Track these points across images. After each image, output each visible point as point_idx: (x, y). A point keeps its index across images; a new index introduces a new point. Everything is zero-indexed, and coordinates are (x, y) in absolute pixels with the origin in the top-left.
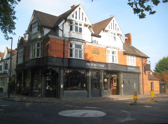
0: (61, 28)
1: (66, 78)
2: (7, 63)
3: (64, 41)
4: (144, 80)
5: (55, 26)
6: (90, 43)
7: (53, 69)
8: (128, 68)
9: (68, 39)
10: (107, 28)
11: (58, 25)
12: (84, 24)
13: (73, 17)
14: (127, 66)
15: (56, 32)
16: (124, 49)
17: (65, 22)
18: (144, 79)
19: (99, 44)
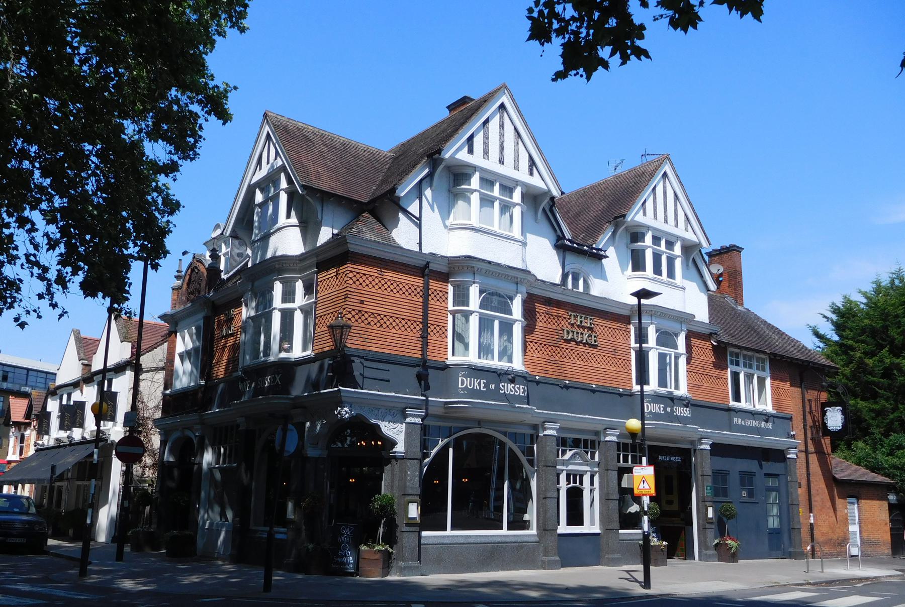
2: (113, 390)
5: (378, 194)
8: (735, 420)
10: (636, 216)
11: (393, 190)
14: (729, 410)
15: (454, 200)
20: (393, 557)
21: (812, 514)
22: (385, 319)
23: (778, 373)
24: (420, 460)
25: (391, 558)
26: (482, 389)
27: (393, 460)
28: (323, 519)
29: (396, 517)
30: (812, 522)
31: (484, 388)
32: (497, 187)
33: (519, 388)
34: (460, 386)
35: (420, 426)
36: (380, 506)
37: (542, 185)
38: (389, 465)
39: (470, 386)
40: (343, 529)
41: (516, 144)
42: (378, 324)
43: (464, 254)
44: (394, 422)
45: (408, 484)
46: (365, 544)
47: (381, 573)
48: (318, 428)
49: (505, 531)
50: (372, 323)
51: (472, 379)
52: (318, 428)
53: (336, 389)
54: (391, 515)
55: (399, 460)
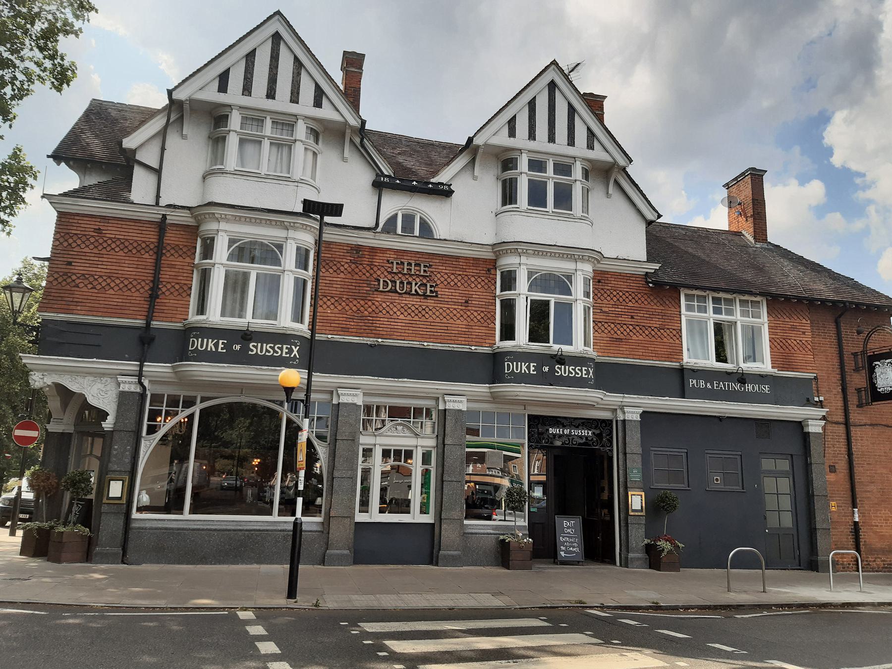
0: (149, 156)
1: (244, 457)
3: (162, 225)
4: (857, 470)
6: (368, 229)
7: (74, 387)
9: (490, 249)
12: (588, 166)
13: (512, 133)
16: (651, 258)
17: (473, 161)
18: (855, 462)
19: (160, 205)
21: (856, 510)
22: (100, 280)
23: (787, 320)
26: (532, 372)
30: (857, 520)
31: (533, 371)
32: (268, 123)
33: (581, 370)
34: (506, 371)
37: (335, 117)
39: (517, 370)
41: (295, 75)
42: (90, 286)
49: (275, 517)
50: (81, 285)
51: (519, 363)
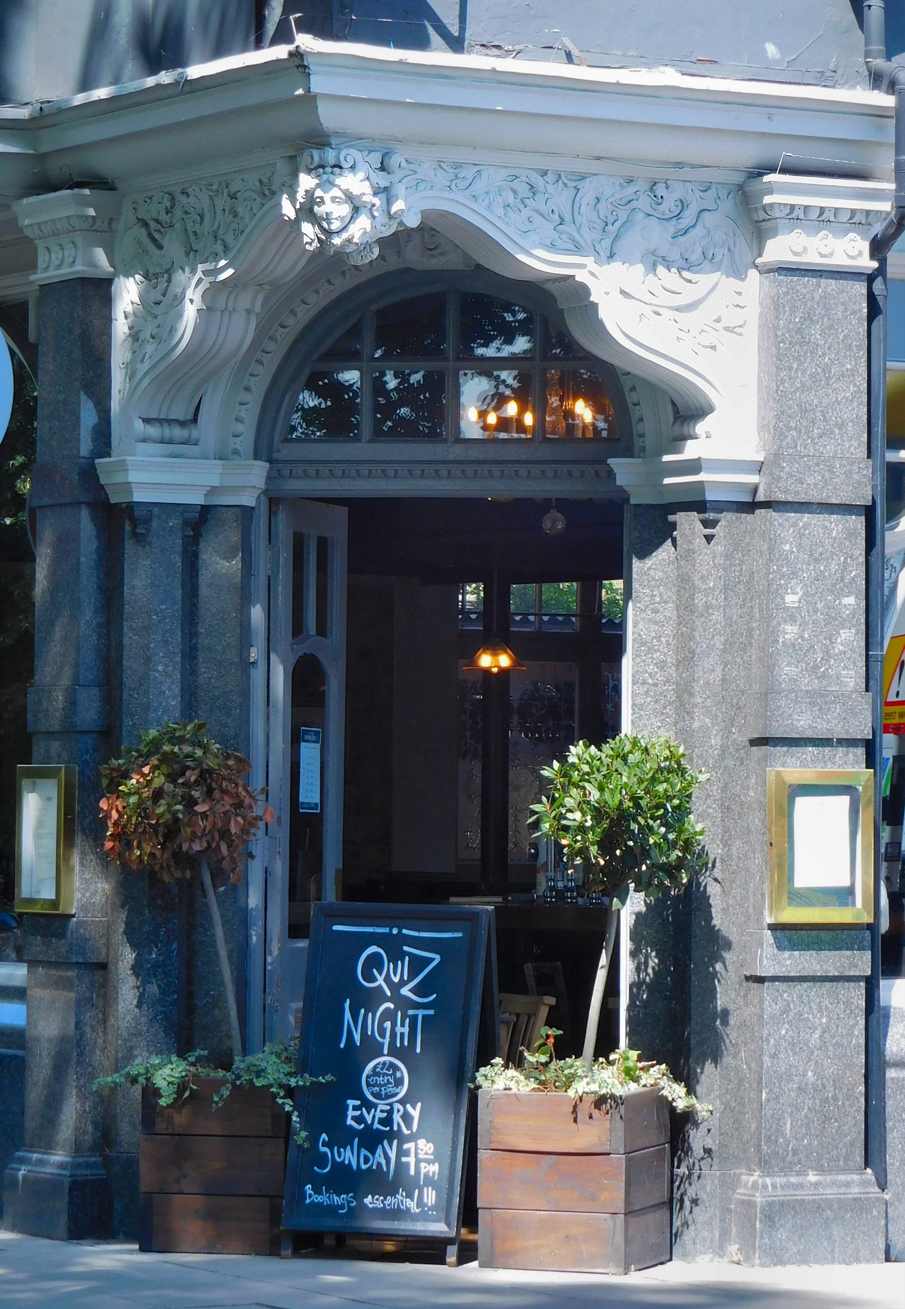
20: (697, 1139)
24: (869, 512)
25: (688, 1151)
27: (680, 518)
28: (254, 900)
29: (713, 890)
35: (861, 288)
36: (598, 813)
38: (665, 552)
40: (375, 962)
43: (756, 381)
44: (686, 265)
45: (787, 670)
46: (515, 1060)
47: (620, 1239)
48: (190, 312)
52: (190, 312)
53: (281, 52)
54: (672, 870)
55: (726, 518)
